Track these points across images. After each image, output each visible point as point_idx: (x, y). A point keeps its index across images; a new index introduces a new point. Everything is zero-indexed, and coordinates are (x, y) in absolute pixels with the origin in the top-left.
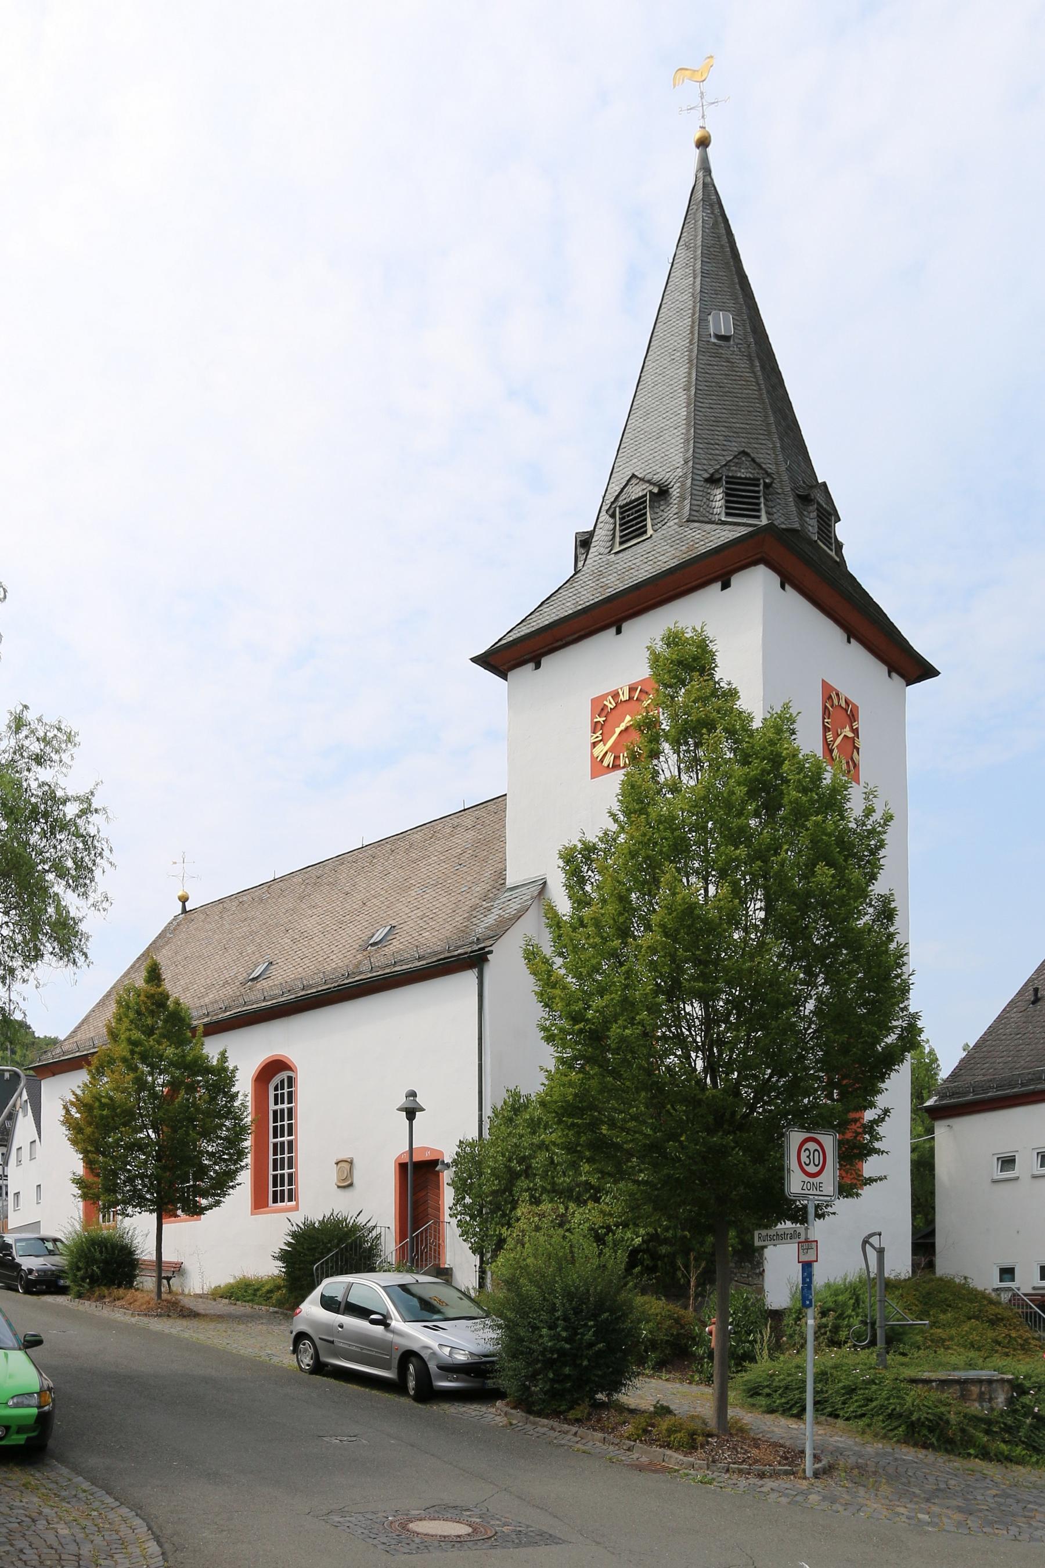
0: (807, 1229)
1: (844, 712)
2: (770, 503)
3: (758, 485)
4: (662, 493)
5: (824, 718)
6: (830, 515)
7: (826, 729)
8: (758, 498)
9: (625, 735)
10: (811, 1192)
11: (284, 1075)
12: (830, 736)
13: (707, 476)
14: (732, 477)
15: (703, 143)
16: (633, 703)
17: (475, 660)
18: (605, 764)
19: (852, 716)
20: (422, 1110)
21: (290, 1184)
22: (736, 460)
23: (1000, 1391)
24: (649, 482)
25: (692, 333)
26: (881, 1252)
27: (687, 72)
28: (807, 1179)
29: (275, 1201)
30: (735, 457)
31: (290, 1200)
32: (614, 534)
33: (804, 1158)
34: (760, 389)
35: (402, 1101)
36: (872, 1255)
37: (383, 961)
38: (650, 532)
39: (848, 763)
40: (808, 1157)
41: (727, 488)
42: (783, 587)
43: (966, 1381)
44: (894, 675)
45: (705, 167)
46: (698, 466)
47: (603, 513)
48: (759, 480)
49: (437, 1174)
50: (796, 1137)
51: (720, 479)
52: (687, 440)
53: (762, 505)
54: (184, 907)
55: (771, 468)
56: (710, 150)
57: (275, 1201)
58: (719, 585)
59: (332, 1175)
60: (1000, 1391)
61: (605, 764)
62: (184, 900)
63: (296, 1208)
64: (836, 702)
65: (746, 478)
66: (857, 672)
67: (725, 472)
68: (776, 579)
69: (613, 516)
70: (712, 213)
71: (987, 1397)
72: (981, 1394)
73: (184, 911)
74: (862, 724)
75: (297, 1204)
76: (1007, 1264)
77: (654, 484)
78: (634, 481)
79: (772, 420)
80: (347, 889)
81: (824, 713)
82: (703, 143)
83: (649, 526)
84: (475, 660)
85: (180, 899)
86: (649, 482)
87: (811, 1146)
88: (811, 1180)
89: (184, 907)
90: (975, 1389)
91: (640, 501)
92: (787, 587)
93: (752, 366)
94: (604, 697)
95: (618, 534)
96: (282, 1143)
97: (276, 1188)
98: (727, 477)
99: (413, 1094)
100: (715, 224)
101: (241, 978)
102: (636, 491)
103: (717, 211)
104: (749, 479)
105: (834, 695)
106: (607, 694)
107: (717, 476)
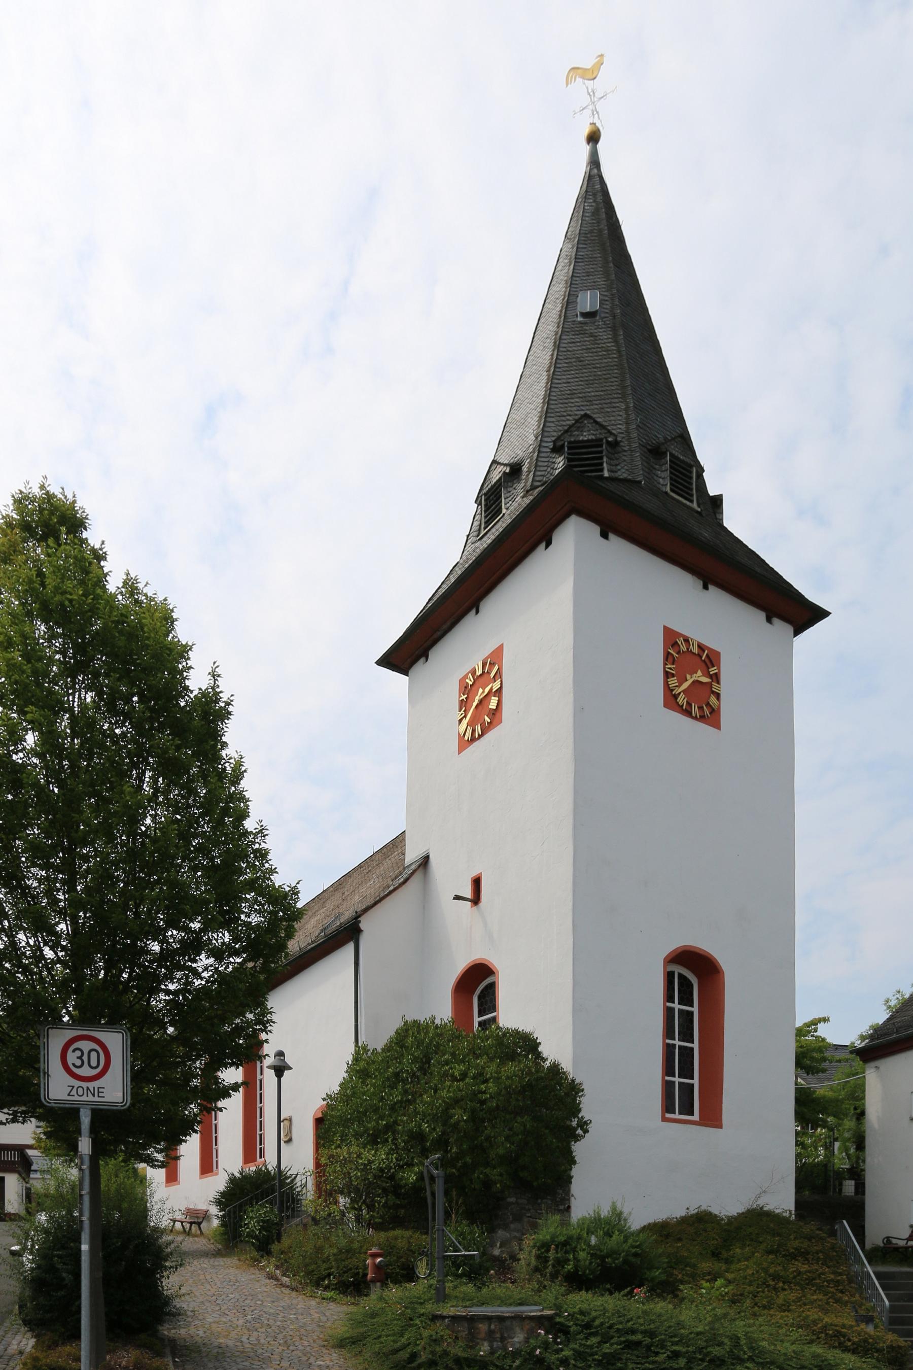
1: (698, 658)
2: (613, 462)
3: (601, 446)
5: (665, 664)
6: (691, 466)
7: (667, 675)
8: (601, 458)
9: (480, 707)
10: (84, 1098)
12: (673, 682)
14: (575, 442)
15: (594, 138)
16: (486, 676)
18: (466, 738)
19: (709, 660)
22: (578, 425)
23: (517, 1329)
25: (560, 316)
27: (579, 71)
28: (77, 1083)
30: (577, 421)
34: (620, 356)
38: (504, 511)
40: (80, 1058)
41: (569, 454)
42: (604, 535)
43: (472, 1320)
44: (776, 621)
45: (594, 162)
46: (546, 439)
48: (601, 440)
51: (563, 446)
52: (540, 417)
53: (605, 465)
56: (600, 146)
58: (543, 545)
60: (517, 1329)
61: (466, 738)
64: (683, 648)
65: (588, 441)
67: (568, 438)
68: (594, 530)
70: (594, 201)
71: (498, 1335)
72: (491, 1333)
79: (628, 383)
82: (594, 138)
87: (86, 1045)
88: (85, 1085)
90: (483, 1327)
92: (611, 536)
94: (466, 676)
98: (569, 443)
100: (596, 212)
103: (600, 198)
104: (592, 440)
105: (680, 641)
106: (467, 674)
107: (559, 443)
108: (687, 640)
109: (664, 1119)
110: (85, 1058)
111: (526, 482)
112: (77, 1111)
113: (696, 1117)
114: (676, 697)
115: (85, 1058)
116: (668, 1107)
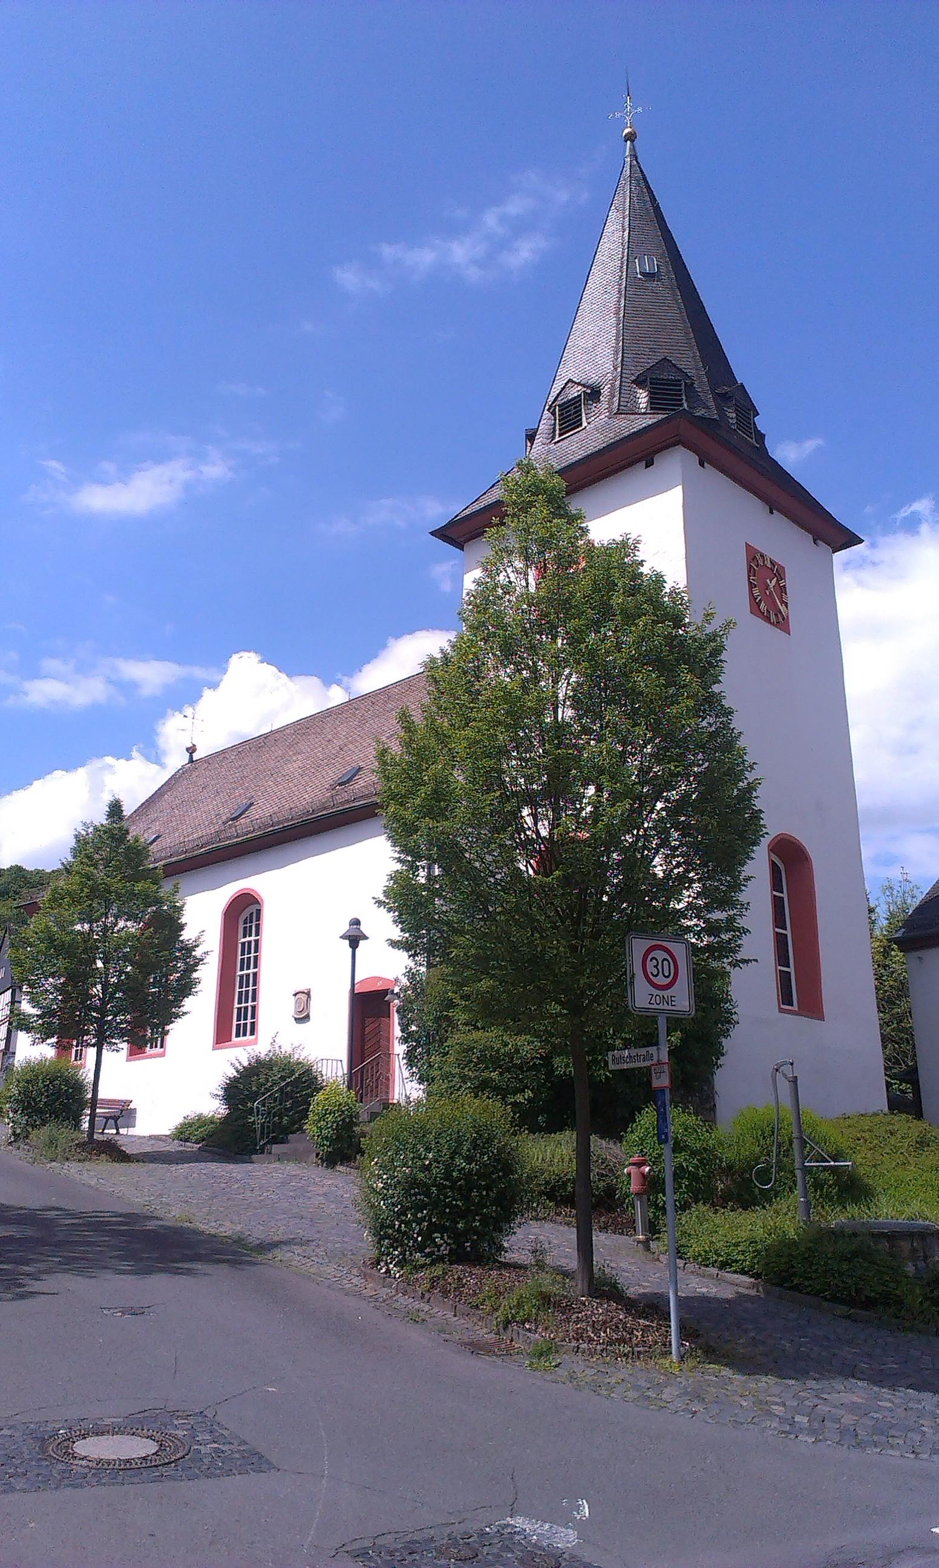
0: (658, 1049)
4: (593, 394)
7: (751, 586)
8: (680, 395)
10: (661, 1006)
11: (253, 908)
13: (633, 378)
17: (432, 533)
19: (779, 573)
20: (366, 938)
21: (253, 1017)
24: (584, 386)
26: (794, 1081)
28: (655, 992)
29: (238, 1035)
31: (252, 1033)
32: (554, 431)
33: (650, 967)
35: (345, 927)
36: (784, 1087)
37: (346, 796)
38: (585, 424)
39: (776, 615)
42: (702, 464)
47: (546, 412)
49: (388, 1003)
50: (638, 946)
51: (645, 381)
54: (191, 757)
55: (691, 372)
57: (238, 1035)
59: (290, 1007)
62: (191, 750)
63: (255, 1042)
66: (781, 540)
69: (553, 414)
72: (914, 1250)
73: (191, 761)
74: (790, 582)
75: (256, 1038)
76: (303, 987)
77: (588, 387)
78: (570, 385)
80: (330, 737)
81: (749, 571)
83: (584, 419)
84: (432, 533)
85: (188, 750)
86: (584, 386)
87: (660, 955)
88: (661, 993)
89: (191, 757)
90: (905, 1245)
91: (576, 401)
93: (675, 295)
95: (557, 427)
96: (248, 975)
97: (235, 1018)
99: (356, 922)
101: (224, 818)
102: (574, 392)
108: (762, 556)
109: (781, 1010)
110: (660, 967)
111: (610, 403)
112: (654, 1019)
113: (795, 1007)
114: (758, 604)
115: (660, 967)
116: (786, 997)
